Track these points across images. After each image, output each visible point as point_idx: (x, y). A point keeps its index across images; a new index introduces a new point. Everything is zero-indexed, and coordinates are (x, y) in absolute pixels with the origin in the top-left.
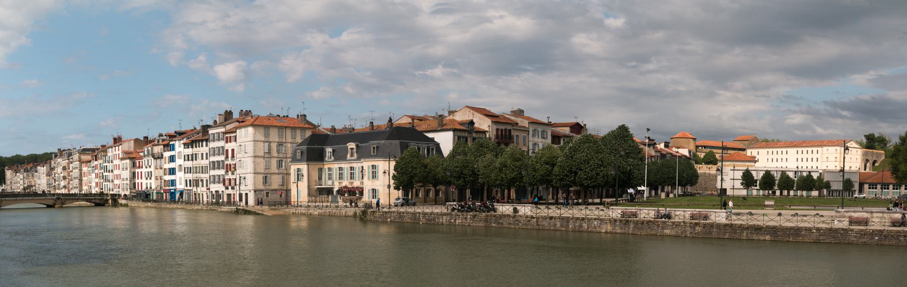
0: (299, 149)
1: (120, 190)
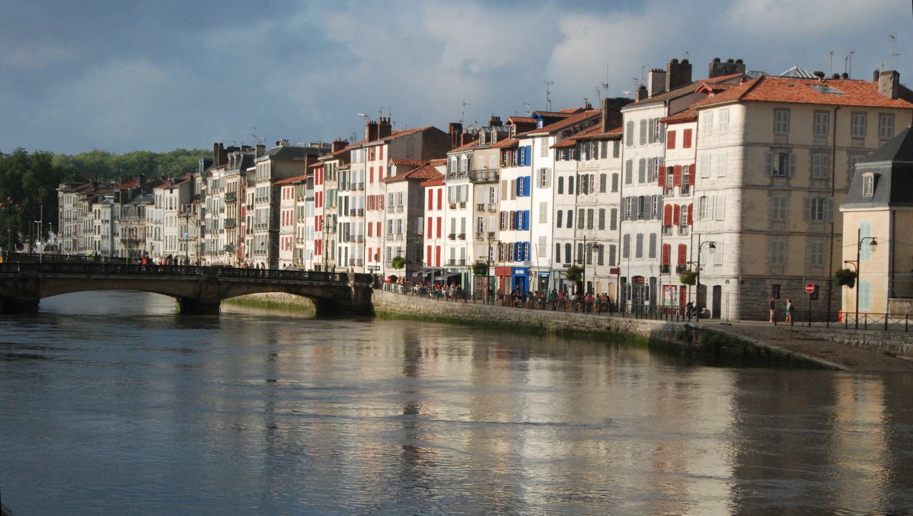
0: (869, 170)
1: (380, 264)
